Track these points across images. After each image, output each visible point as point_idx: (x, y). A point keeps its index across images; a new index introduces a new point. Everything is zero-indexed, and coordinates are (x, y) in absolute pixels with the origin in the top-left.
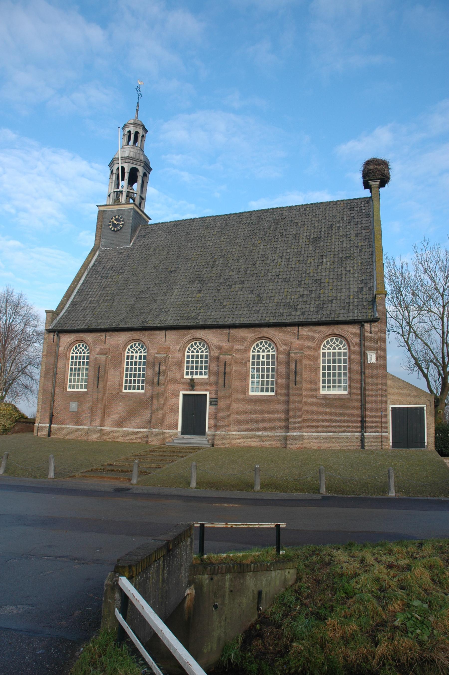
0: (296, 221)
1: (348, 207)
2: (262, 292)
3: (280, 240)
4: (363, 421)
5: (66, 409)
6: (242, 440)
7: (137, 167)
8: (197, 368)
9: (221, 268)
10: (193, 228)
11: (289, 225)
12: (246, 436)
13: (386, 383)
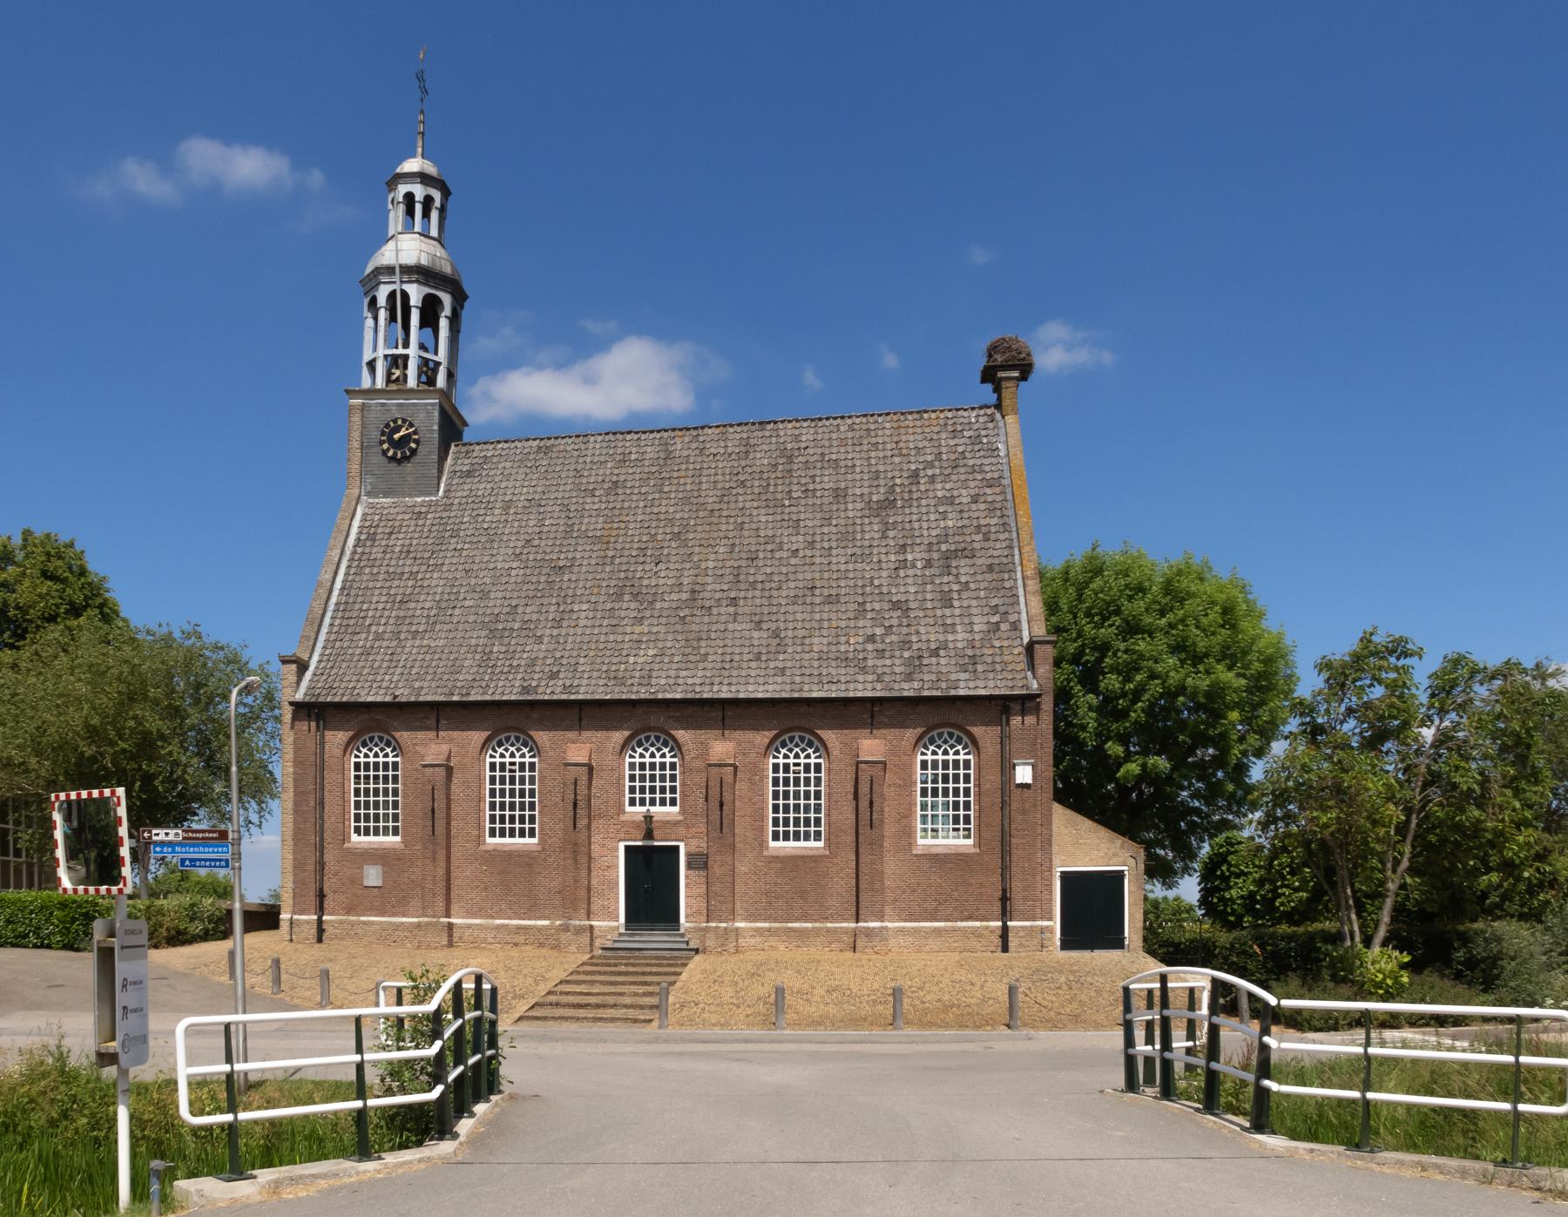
0: (834, 457)
1: (950, 428)
2: (782, 626)
3: (803, 502)
4: (1004, 899)
5: (356, 880)
6: (758, 939)
7: (441, 294)
8: (653, 790)
9: (678, 566)
10: (588, 459)
11: (819, 465)
12: (769, 930)
13: (1050, 823)
